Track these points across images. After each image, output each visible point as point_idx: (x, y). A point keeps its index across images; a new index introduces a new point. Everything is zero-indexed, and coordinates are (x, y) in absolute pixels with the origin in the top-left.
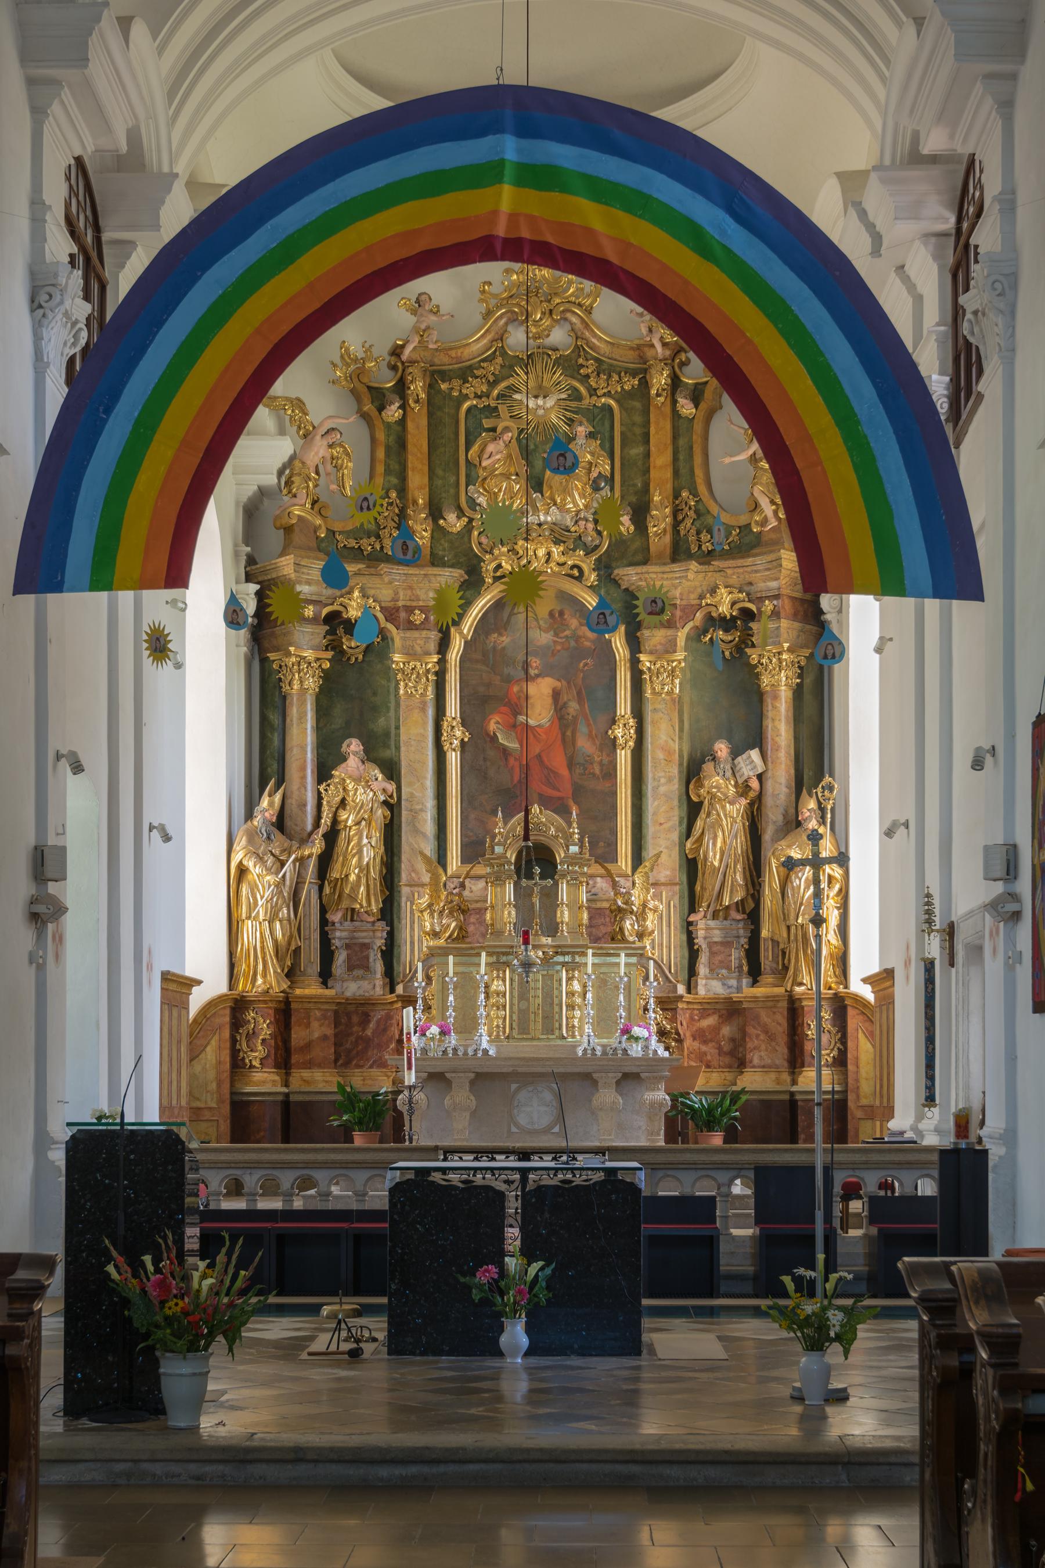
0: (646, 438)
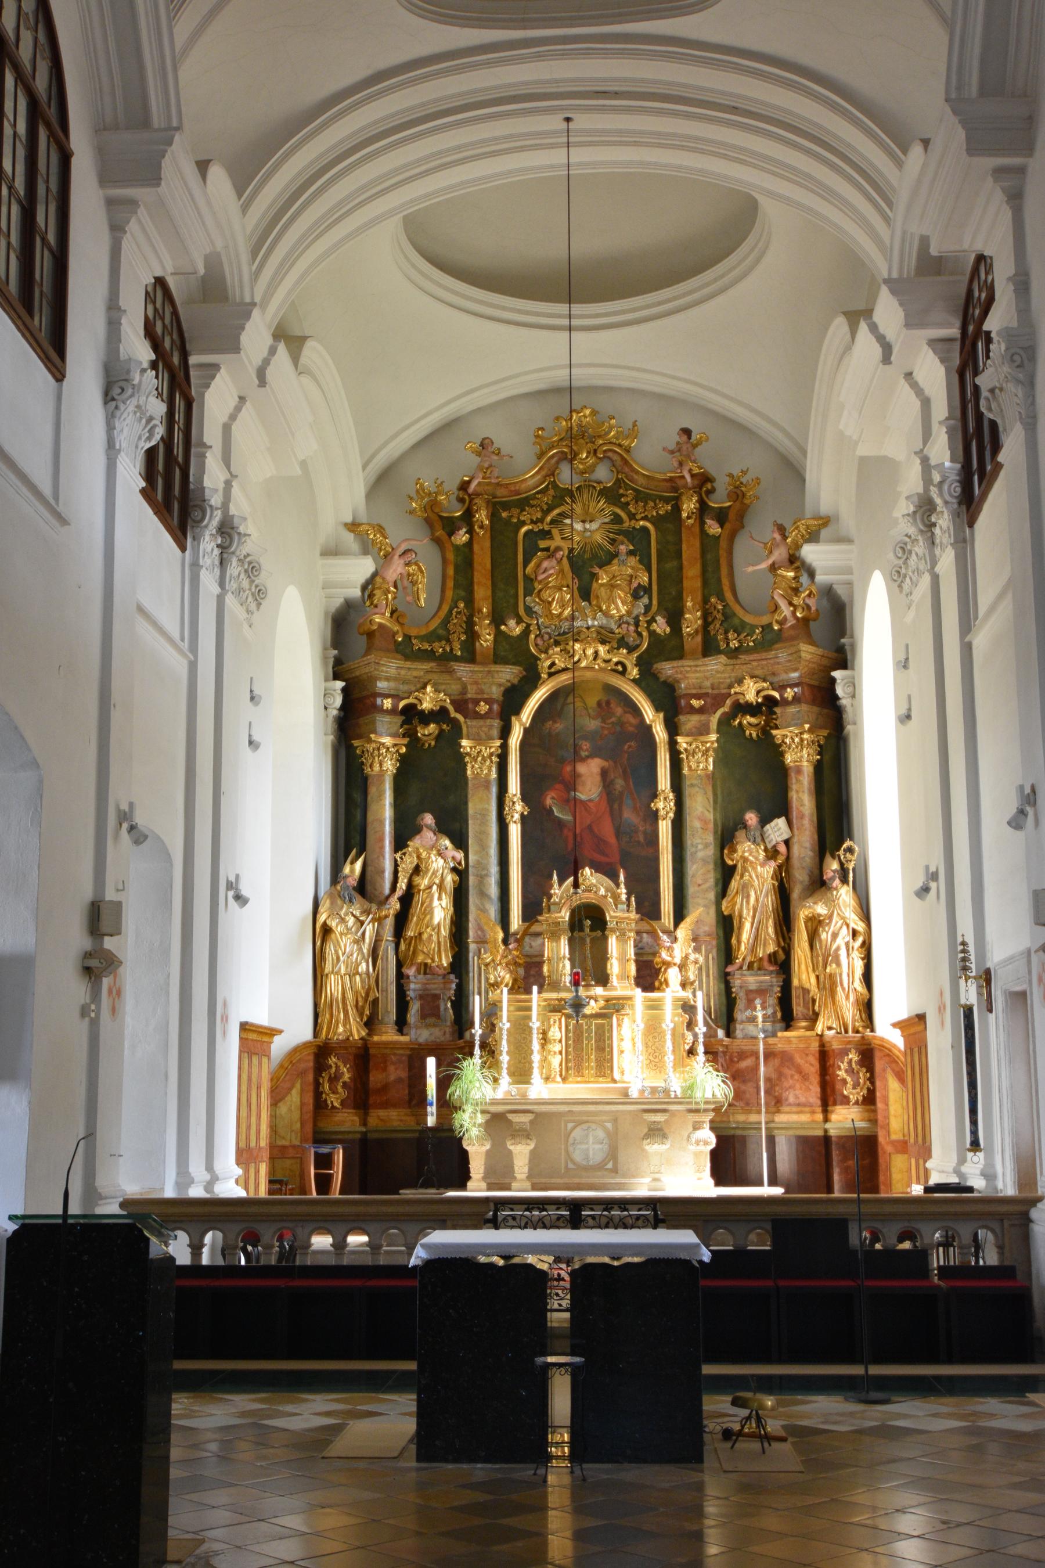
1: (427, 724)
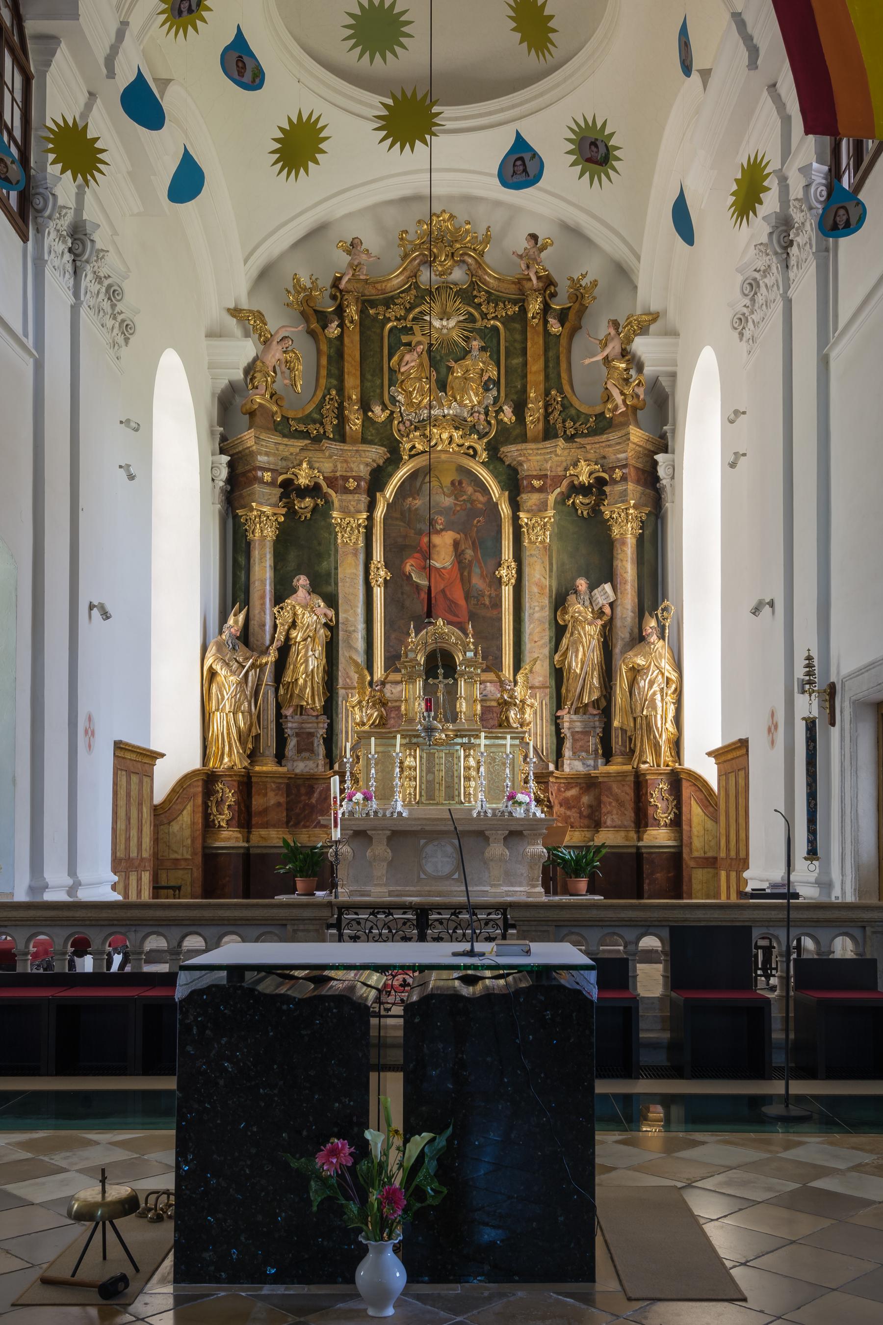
1: (303, 498)
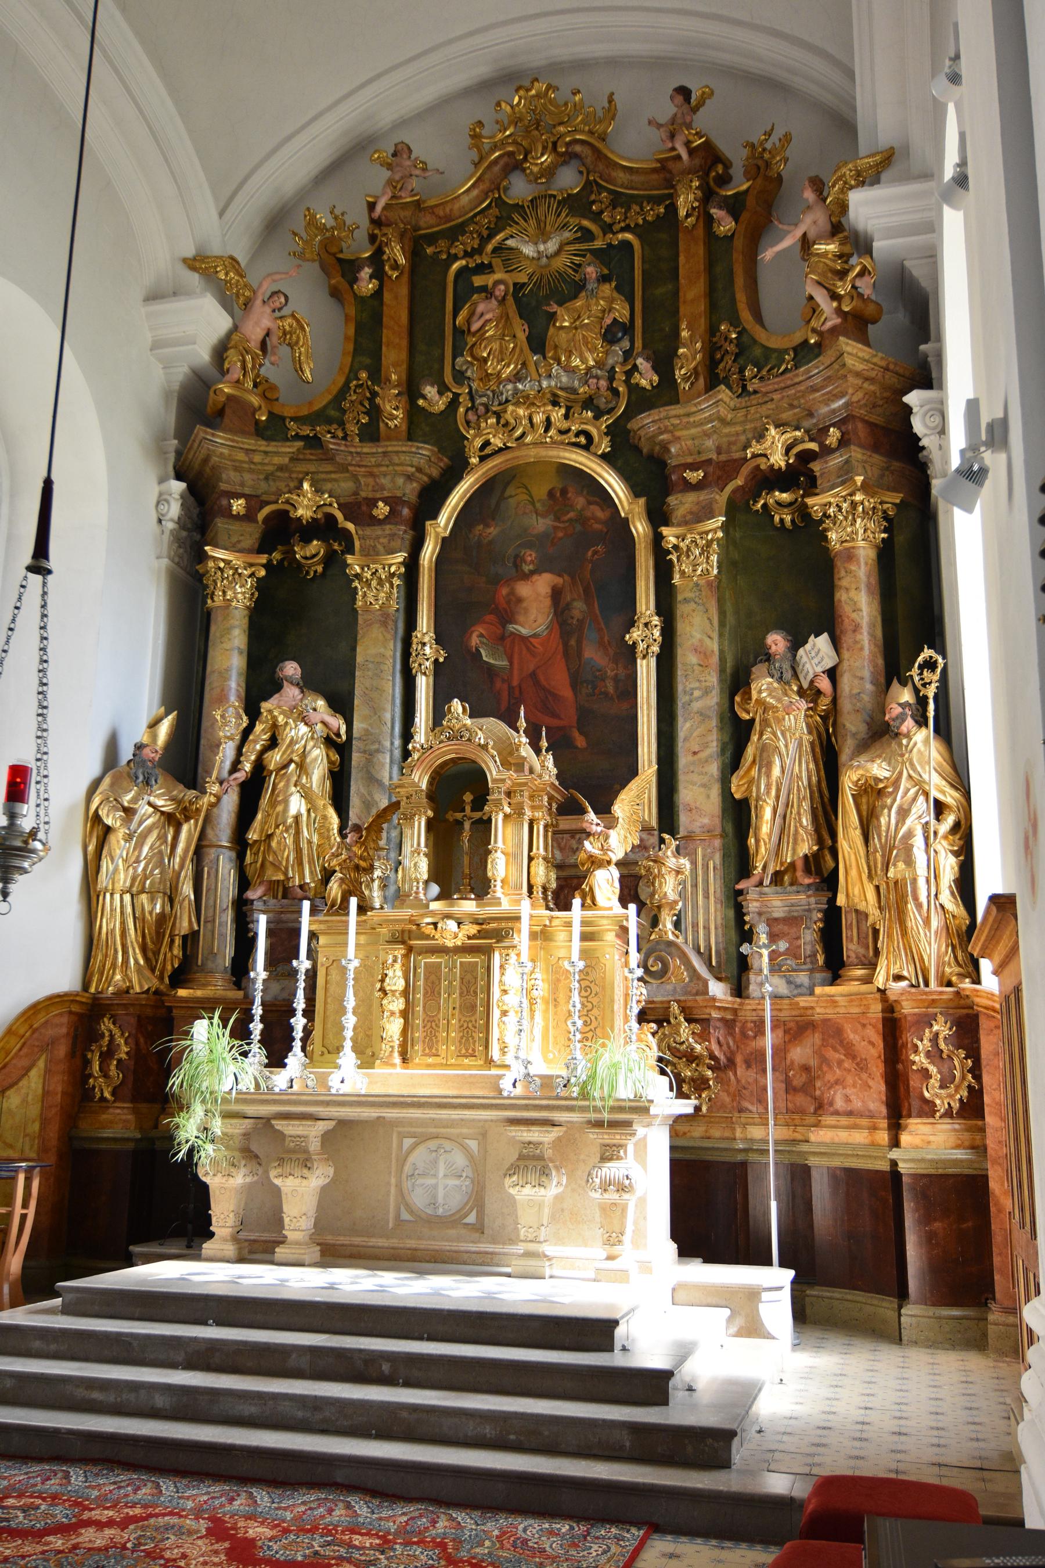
0: (674, 274)
1: (307, 540)
